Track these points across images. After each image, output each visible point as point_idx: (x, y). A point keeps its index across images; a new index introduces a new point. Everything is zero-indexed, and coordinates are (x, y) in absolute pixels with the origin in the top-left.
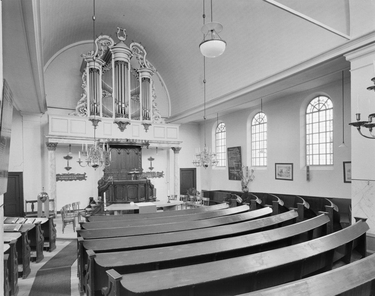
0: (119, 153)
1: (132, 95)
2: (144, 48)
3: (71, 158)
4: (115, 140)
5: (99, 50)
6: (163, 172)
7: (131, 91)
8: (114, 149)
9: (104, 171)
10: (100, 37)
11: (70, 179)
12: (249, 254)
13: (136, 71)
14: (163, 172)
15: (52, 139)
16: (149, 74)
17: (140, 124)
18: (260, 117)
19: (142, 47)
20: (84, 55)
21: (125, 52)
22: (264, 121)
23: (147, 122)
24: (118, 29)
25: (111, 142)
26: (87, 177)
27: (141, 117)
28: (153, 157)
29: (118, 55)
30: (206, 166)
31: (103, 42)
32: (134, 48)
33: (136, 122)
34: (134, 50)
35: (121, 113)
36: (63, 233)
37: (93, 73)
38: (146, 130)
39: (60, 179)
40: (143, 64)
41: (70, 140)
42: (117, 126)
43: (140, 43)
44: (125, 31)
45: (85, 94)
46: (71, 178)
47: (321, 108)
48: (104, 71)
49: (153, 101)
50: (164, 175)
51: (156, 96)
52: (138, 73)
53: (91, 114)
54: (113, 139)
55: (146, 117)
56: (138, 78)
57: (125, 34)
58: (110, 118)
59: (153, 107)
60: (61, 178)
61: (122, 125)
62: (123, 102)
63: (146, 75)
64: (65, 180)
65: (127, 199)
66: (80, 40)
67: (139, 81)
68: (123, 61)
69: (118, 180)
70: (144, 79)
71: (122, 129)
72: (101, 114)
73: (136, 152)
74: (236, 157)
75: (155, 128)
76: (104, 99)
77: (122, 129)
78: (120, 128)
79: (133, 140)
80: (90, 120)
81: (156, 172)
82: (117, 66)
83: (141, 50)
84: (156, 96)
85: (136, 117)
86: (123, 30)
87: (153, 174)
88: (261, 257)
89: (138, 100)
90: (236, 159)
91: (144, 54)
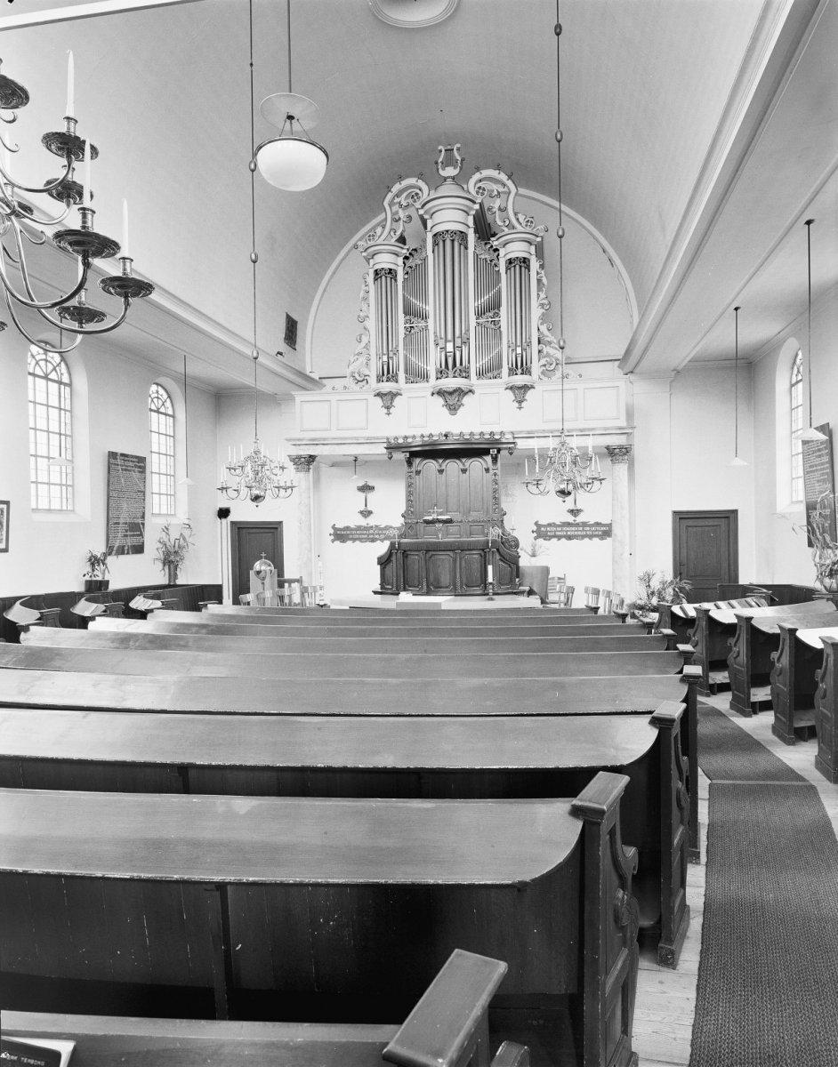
0: (441, 471)
1: (479, 314)
3: (372, 488)
4: (487, 436)
8: (473, 459)
10: (396, 188)
13: (492, 246)
15: (301, 447)
17: (502, 390)
21: (458, 207)
23: (520, 380)
24: (441, 151)
26: (533, 532)
27: (505, 370)
29: (438, 217)
31: (403, 200)
32: (479, 188)
35: (452, 366)
37: (513, 269)
38: (520, 402)
39: (351, 536)
40: (507, 222)
42: (440, 401)
43: (498, 168)
44: (458, 149)
52: (496, 250)
53: (379, 380)
55: (522, 367)
56: (496, 266)
57: (459, 158)
58: (425, 384)
61: (453, 399)
64: (361, 540)
65: (428, 587)
68: (447, 231)
70: (510, 263)
71: (453, 409)
72: (402, 376)
74: (819, 465)
77: (453, 409)
79: (492, 434)
80: (378, 395)
82: (441, 244)
84: (550, 303)
85: (490, 371)
90: (821, 470)
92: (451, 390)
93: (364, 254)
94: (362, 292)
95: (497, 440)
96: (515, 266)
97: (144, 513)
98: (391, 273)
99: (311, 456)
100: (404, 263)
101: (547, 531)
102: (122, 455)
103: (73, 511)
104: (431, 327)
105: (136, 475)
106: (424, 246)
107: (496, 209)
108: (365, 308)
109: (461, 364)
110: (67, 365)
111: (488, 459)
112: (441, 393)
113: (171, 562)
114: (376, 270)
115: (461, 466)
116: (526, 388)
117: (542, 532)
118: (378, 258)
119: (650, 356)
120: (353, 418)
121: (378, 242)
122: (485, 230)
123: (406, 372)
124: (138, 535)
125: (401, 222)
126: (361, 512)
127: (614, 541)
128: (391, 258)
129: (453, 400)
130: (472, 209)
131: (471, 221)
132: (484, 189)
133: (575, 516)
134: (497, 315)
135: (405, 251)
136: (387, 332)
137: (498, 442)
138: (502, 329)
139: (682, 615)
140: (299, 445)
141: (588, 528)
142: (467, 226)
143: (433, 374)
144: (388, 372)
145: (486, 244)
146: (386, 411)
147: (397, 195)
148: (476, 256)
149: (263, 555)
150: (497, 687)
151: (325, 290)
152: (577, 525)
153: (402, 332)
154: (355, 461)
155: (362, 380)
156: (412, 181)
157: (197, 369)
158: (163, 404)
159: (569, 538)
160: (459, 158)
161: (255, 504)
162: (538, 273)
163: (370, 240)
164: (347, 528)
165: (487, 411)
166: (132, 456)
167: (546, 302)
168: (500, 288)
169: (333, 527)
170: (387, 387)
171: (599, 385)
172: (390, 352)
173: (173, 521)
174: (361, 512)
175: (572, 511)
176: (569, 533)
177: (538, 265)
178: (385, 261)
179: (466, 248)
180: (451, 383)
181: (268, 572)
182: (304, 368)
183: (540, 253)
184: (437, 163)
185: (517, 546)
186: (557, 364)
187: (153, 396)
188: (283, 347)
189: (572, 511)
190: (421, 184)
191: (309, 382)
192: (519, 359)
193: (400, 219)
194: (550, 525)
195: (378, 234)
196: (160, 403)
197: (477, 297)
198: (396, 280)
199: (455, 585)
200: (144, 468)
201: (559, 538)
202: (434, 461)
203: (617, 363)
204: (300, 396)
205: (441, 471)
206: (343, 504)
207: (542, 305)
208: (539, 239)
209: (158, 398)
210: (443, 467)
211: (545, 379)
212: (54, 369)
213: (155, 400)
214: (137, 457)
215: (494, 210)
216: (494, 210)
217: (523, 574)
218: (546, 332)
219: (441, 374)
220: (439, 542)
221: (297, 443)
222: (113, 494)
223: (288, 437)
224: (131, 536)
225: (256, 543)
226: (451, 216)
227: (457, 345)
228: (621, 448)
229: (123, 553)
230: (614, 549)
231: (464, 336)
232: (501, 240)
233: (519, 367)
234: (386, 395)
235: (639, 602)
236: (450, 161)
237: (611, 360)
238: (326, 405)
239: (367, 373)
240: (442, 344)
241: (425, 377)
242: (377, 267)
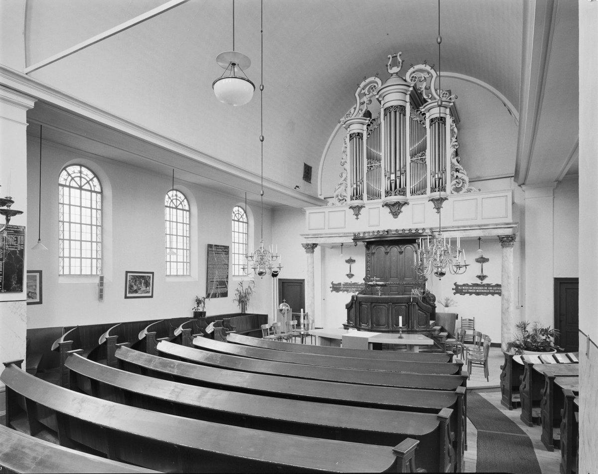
1: (412, 156)
3: (487, 260)
4: (414, 231)
10: (417, 67)
12: (312, 437)
13: (421, 112)
15: (309, 239)
17: (347, 209)
18: (172, 198)
21: (395, 91)
22: (180, 200)
24: (389, 58)
25: (414, 234)
26: (453, 289)
27: (428, 189)
28: (485, 256)
29: (387, 98)
30: (442, 274)
32: (413, 77)
33: (418, 199)
35: (397, 188)
36: (488, 381)
41: (326, 238)
42: (387, 210)
43: (425, 63)
44: (400, 55)
47: (78, 184)
52: (424, 114)
53: (352, 199)
54: (403, 230)
55: (440, 186)
57: (400, 61)
58: (379, 200)
61: (395, 209)
66: (457, 71)
68: (392, 106)
69: (385, 295)
71: (395, 214)
72: (365, 196)
75: (371, 210)
76: (370, 172)
77: (395, 214)
79: (417, 230)
80: (351, 208)
81: (342, 283)
82: (388, 114)
85: (419, 190)
87: (486, 288)
88: (83, 401)
89: (423, 160)
92: (393, 203)
93: (344, 126)
94: (343, 148)
95: (420, 233)
97: (228, 276)
98: (360, 135)
99: (314, 244)
100: (367, 128)
101: (462, 289)
102: (215, 246)
103: (190, 275)
104: (383, 166)
105: (223, 256)
106: (379, 117)
109: (400, 187)
110: (187, 200)
111: (416, 245)
112: (387, 205)
113: (242, 302)
115: (399, 250)
116: (441, 200)
117: (459, 290)
118: (352, 127)
119: (531, 173)
120: (337, 221)
121: (353, 117)
122: (417, 100)
124: (224, 287)
125: (365, 104)
126: (347, 275)
127: (502, 299)
128: (359, 126)
129: (395, 209)
131: (408, 98)
132: (416, 78)
133: (482, 280)
134: (424, 154)
135: (367, 121)
136: (357, 170)
137: (420, 235)
138: (427, 163)
139: (521, 362)
140: (308, 238)
141: (491, 288)
142: (405, 101)
143: (383, 194)
144: (357, 194)
145: (417, 111)
146: (356, 217)
147: (363, 89)
148: (411, 119)
149: (284, 300)
150: (262, 438)
151: (329, 148)
152: (484, 286)
154: (342, 246)
155: (342, 199)
156: (372, 79)
157: (251, 197)
158: (242, 217)
159: (478, 294)
160: (400, 61)
161: (261, 277)
162: (451, 126)
163: (347, 117)
166: (221, 246)
169: (332, 283)
170: (356, 203)
171: (492, 195)
172: (358, 181)
173: (246, 279)
174: (347, 275)
175: (479, 277)
176: (477, 291)
177: (451, 120)
178: (355, 128)
179: (404, 115)
180: (393, 199)
181: (286, 310)
182: (317, 194)
183: (454, 112)
184: (387, 66)
185: (434, 300)
186: (463, 183)
187: (236, 213)
188: (301, 182)
189: (479, 277)
190: (378, 80)
191: (318, 201)
193: (364, 102)
194: (464, 285)
196: (240, 216)
197: (411, 144)
198: (362, 139)
199: (388, 324)
200: (228, 252)
201: (471, 294)
202: (382, 247)
203: (513, 178)
204: (309, 210)
205: (387, 253)
206: (338, 270)
207: (454, 146)
208: (452, 104)
209: (239, 214)
211: (455, 193)
212: (181, 203)
213: (237, 215)
214: (224, 246)
215: (422, 90)
216: (422, 90)
217: (438, 317)
218: (456, 163)
219: (388, 193)
220: (379, 298)
221: (307, 236)
222: (210, 266)
223: (301, 234)
224: (220, 288)
225: (292, 293)
226: (394, 97)
227: (397, 176)
228: (508, 237)
229: (215, 297)
230: (502, 305)
231: (403, 170)
232: (426, 108)
234: (355, 207)
235: (518, 342)
237: (509, 177)
238: (323, 214)
239: (345, 194)
242: (351, 133)
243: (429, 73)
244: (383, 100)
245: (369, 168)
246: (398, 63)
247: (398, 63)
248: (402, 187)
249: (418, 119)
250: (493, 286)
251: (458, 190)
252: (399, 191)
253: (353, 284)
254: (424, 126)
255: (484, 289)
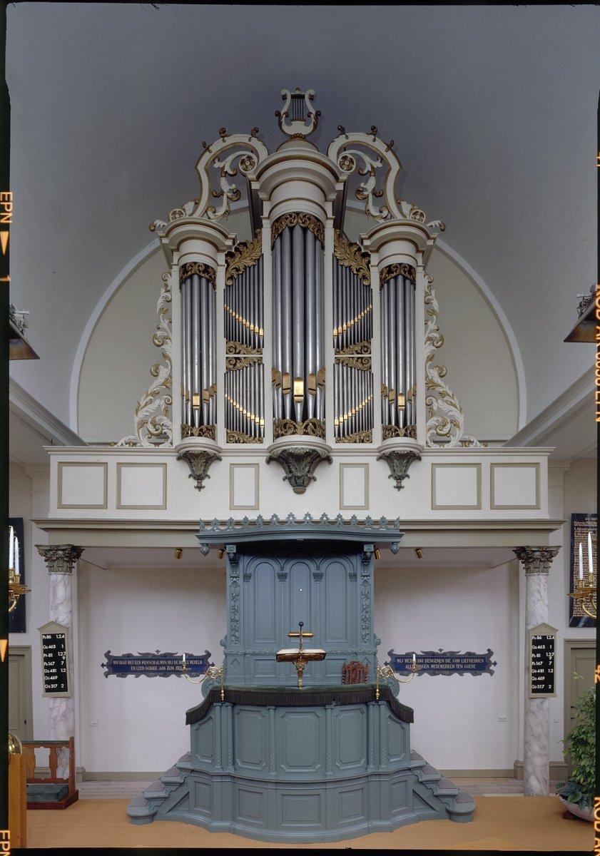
1: (340, 346)
2: (390, 147)
5: (211, 192)
6: (490, 653)
7: (335, 332)
9: (222, 644)
10: (355, 137)
11: (162, 671)
13: (359, 249)
14: (490, 653)
16: (412, 246)
17: (171, 461)
19: (380, 146)
20: (159, 223)
24: (284, 98)
26: (103, 665)
27: (377, 431)
29: (280, 194)
31: (227, 165)
32: (345, 158)
34: (347, 163)
37: (392, 281)
38: (399, 478)
43: (374, 131)
44: (311, 98)
45: (166, 366)
46: (163, 668)
48: (234, 272)
49: (430, 358)
50: (495, 664)
51: (442, 339)
53: (185, 432)
55: (401, 425)
56: (364, 277)
59: (431, 385)
60: (134, 665)
61: (299, 468)
62: (299, 372)
63: (398, 253)
67: (369, 286)
68: (298, 214)
71: (299, 484)
72: (221, 430)
73: (350, 570)
77: (299, 484)
78: (290, 479)
83: (376, 156)
84: (442, 339)
85: (357, 429)
86: (303, 97)
87: (448, 661)
89: (365, 365)
91: (390, 170)
96: (396, 278)
100: (226, 262)
107: (369, 192)
108: (164, 324)
114: (184, 266)
123: (227, 426)
130: (333, 190)
134: (367, 349)
141: (458, 661)
148: (336, 261)
153: (222, 369)
164: (129, 656)
165: (350, 491)
167: (436, 335)
168: (371, 311)
169: (107, 655)
170: (199, 443)
178: (197, 252)
179: (323, 247)
184: (278, 114)
192: (299, 408)
195: (189, 212)
210: (323, 570)
216: (365, 193)
219: (282, 428)
227: (199, 397)
233: (299, 417)
236: (298, 114)
238: (101, 469)
240: (286, 382)
241: (257, 435)
243: (383, 160)
244: (269, 199)
245: (233, 364)
246: (306, 117)
247: (306, 117)
248: (211, 424)
249: (353, 264)
250: (461, 657)
251: (441, 440)
252: (208, 429)
253: (161, 656)
254: (366, 283)
255: (445, 663)
